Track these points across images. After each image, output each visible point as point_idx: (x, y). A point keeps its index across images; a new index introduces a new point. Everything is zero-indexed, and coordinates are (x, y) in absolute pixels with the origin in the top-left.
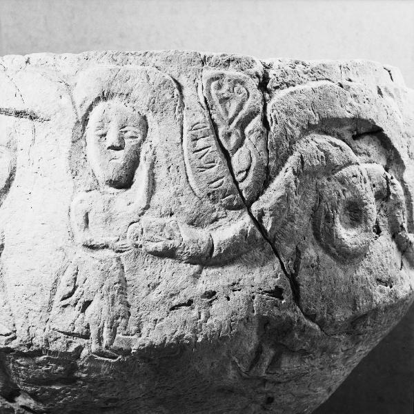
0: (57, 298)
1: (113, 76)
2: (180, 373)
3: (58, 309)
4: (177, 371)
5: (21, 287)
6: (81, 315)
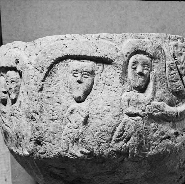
0: (114, 136)
1: (139, 43)
2: (160, 167)
3: (114, 142)
4: (159, 166)
5: (97, 132)
6: (125, 144)
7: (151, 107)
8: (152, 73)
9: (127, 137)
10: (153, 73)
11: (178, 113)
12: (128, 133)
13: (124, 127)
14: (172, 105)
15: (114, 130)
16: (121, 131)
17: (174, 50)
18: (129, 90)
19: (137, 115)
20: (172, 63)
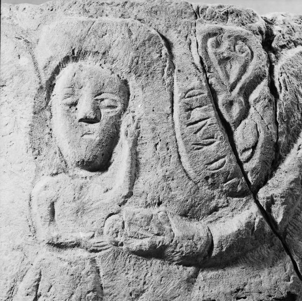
1: (86, 29)
17: (205, 49)
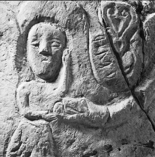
7: (62, 106)
8: (65, 52)
9: (25, 151)
10: (67, 51)
11: (111, 115)
12: (26, 145)
13: (20, 136)
14: (101, 103)
15: (8, 140)
16: (16, 142)
18: (28, 79)
19: (39, 117)
20: (99, 36)
